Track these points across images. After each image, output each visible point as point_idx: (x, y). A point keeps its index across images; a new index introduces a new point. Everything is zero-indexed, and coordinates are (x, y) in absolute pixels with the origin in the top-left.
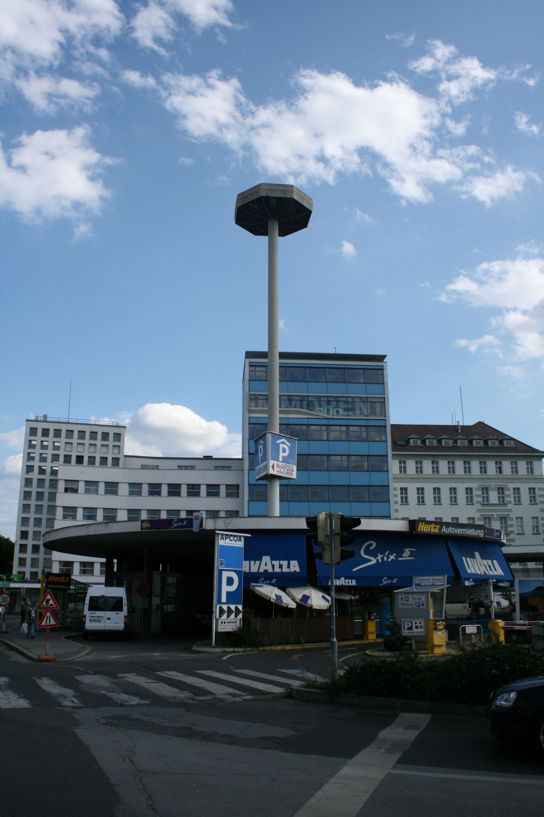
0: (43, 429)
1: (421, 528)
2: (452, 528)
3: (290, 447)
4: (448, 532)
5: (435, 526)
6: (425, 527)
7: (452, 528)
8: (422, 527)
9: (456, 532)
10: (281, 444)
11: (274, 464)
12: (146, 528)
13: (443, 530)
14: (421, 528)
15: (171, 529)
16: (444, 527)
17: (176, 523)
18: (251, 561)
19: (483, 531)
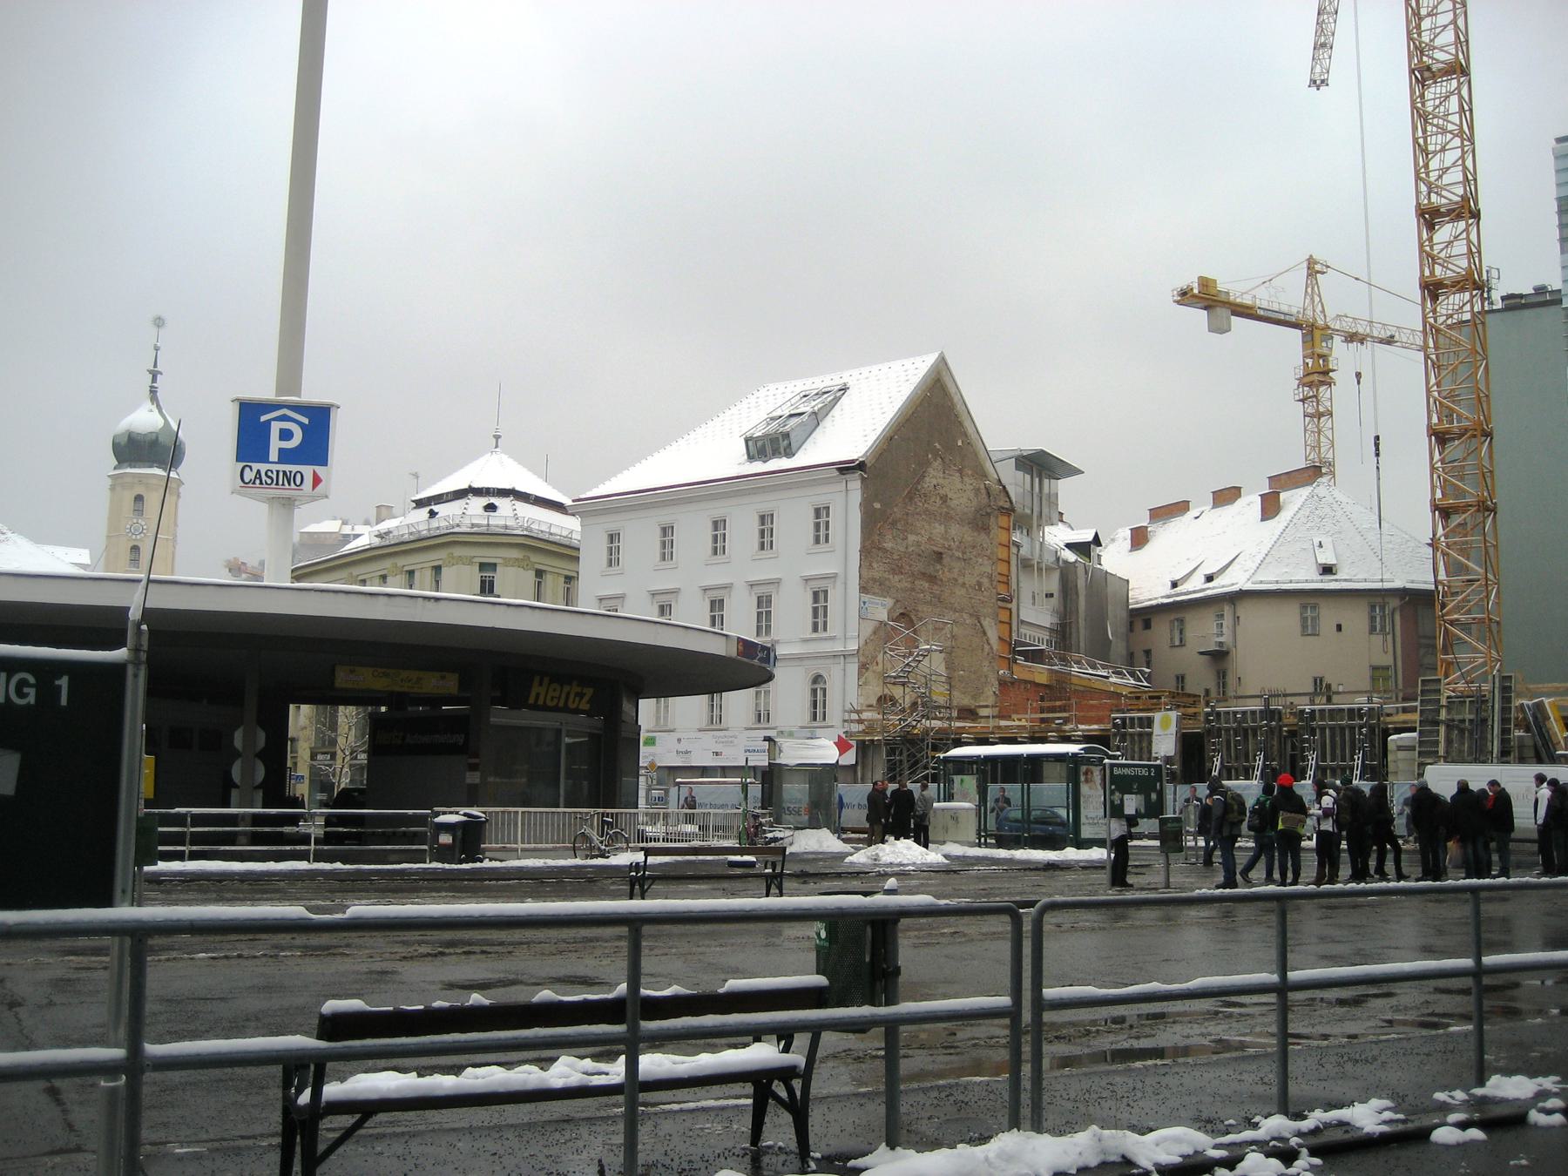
0: (281, 438)
1: (538, 695)
3: (1563, 1079)
6: (551, 693)
8: (542, 691)
10: (273, 423)
11: (314, 488)
14: (538, 695)
18: (1537, 845)
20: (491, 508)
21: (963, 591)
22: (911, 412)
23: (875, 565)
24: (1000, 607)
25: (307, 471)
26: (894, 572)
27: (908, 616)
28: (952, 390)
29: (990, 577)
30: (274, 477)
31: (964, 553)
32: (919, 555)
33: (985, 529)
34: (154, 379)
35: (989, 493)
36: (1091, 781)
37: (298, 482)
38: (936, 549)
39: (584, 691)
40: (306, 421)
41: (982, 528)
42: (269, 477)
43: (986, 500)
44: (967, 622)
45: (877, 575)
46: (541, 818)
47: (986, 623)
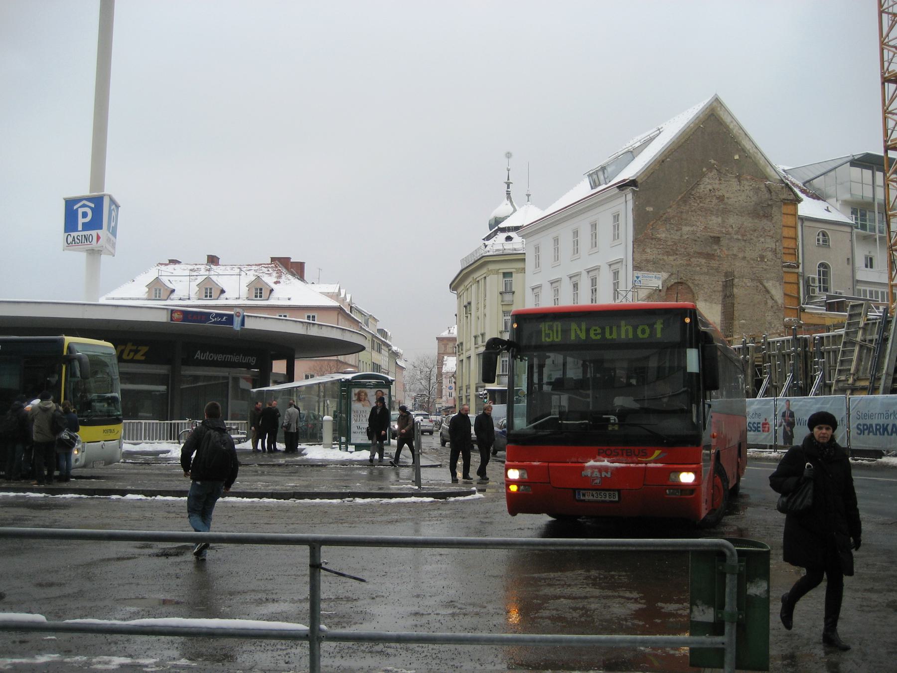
0: (83, 218)
2: (210, 353)
4: (204, 358)
5: (134, 348)
7: (210, 353)
9: (215, 359)
11: (98, 234)
12: (177, 320)
13: (196, 356)
15: (211, 323)
16: (199, 352)
17: (214, 318)
19: (255, 358)
20: (509, 239)
21: (744, 263)
22: (683, 141)
23: (648, 250)
24: (785, 272)
25: (94, 233)
26: (668, 254)
27: (685, 284)
28: (727, 120)
29: (774, 252)
30: (80, 239)
31: (743, 235)
32: (696, 241)
33: (768, 216)
34: (508, 187)
35: (770, 190)
36: (365, 400)
37: (90, 241)
38: (712, 235)
39: (139, 348)
40: (93, 205)
41: (764, 216)
42: (79, 239)
43: (767, 196)
44: (748, 284)
45: (650, 257)
46: (129, 427)
47: (769, 285)
